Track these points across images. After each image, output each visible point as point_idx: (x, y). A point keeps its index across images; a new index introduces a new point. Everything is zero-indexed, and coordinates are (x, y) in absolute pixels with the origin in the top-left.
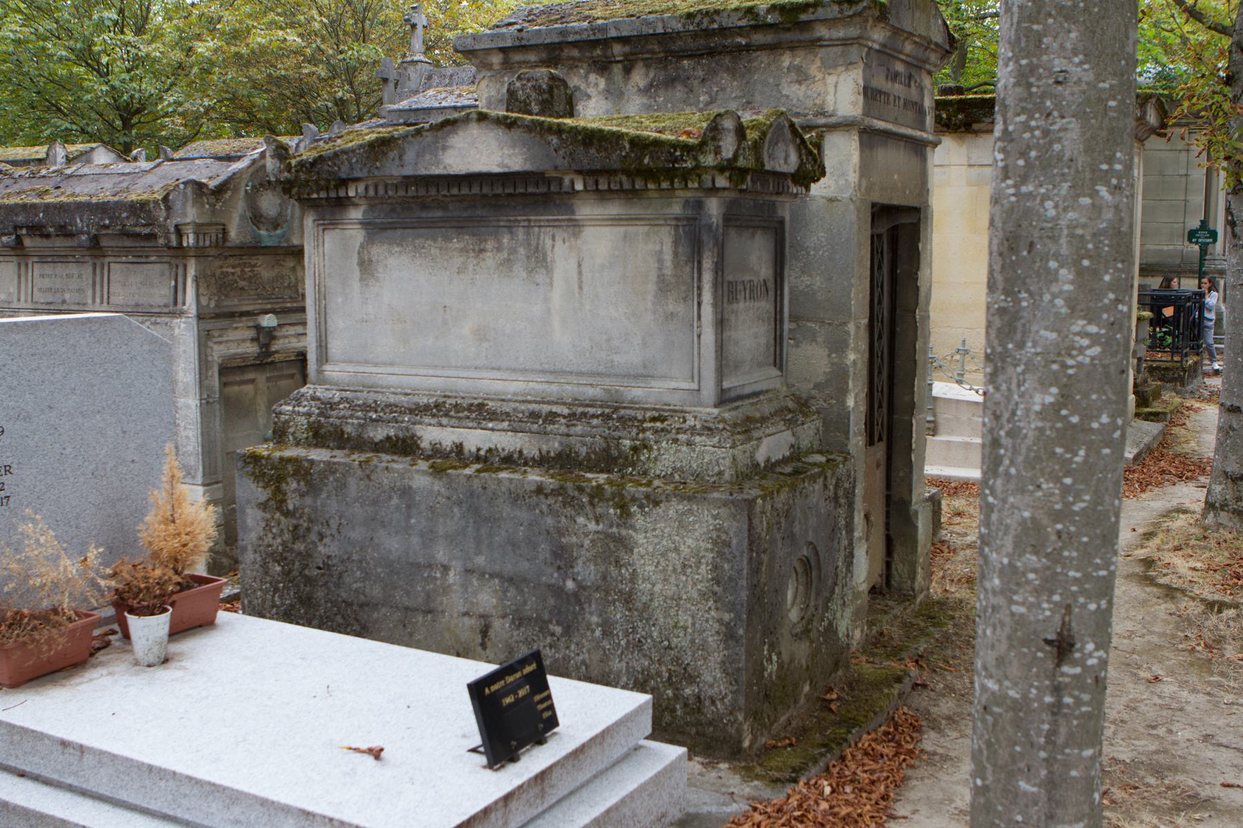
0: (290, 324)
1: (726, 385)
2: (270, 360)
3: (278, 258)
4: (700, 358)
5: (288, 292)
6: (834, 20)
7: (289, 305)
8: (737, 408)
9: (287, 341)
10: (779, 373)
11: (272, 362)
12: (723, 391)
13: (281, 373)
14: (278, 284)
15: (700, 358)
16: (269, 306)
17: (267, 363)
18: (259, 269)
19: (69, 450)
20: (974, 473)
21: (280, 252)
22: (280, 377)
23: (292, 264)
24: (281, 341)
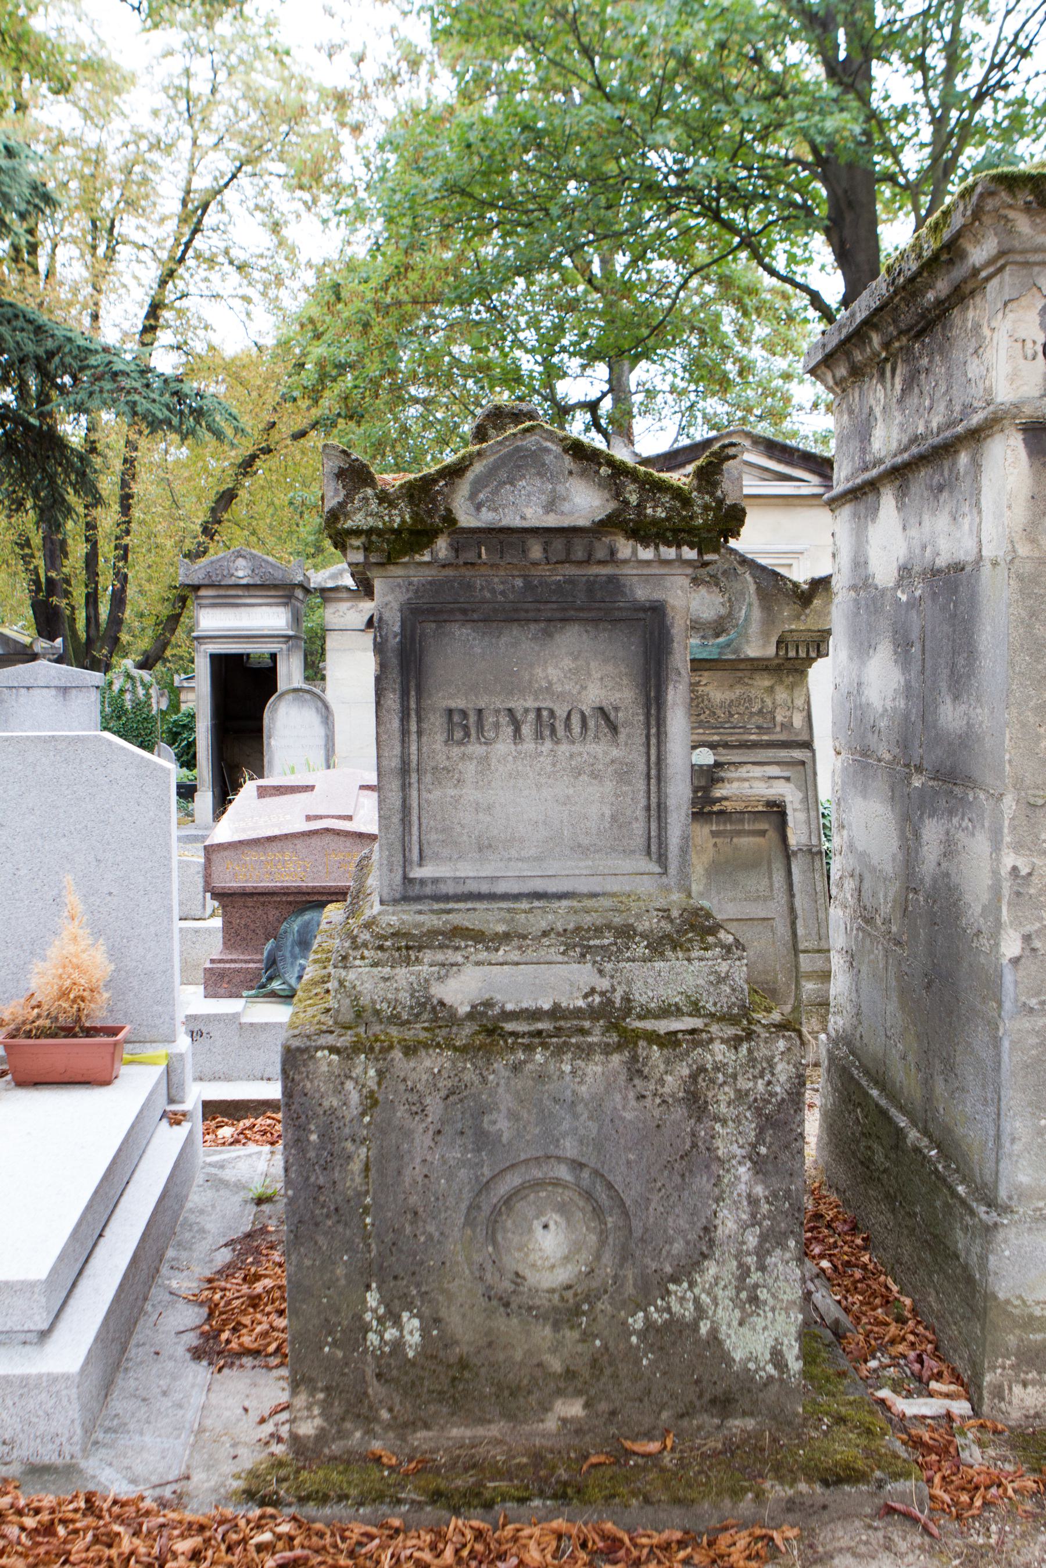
0: (754, 763)
1: (417, 873)
2: (715, 808)
3: (740, 674)
4: (321, 817)
5: (759, 720)
6: (932, 202)
7: (753, 737)
8: (449, 912)
9: (746, 784)
10: (657, 869)
11: (721, 812)
12: (407, 880)
13: (739, 827)
14: (741, 709)
15: (321, 817)
16: (716, 738)
17: (711, 813)
18: (706, 689)
19: (22, 872)
20: (273, 1091)
21: (742, 666)
22: (739, 833)
23: (767, 683)
24: (735, 785)
